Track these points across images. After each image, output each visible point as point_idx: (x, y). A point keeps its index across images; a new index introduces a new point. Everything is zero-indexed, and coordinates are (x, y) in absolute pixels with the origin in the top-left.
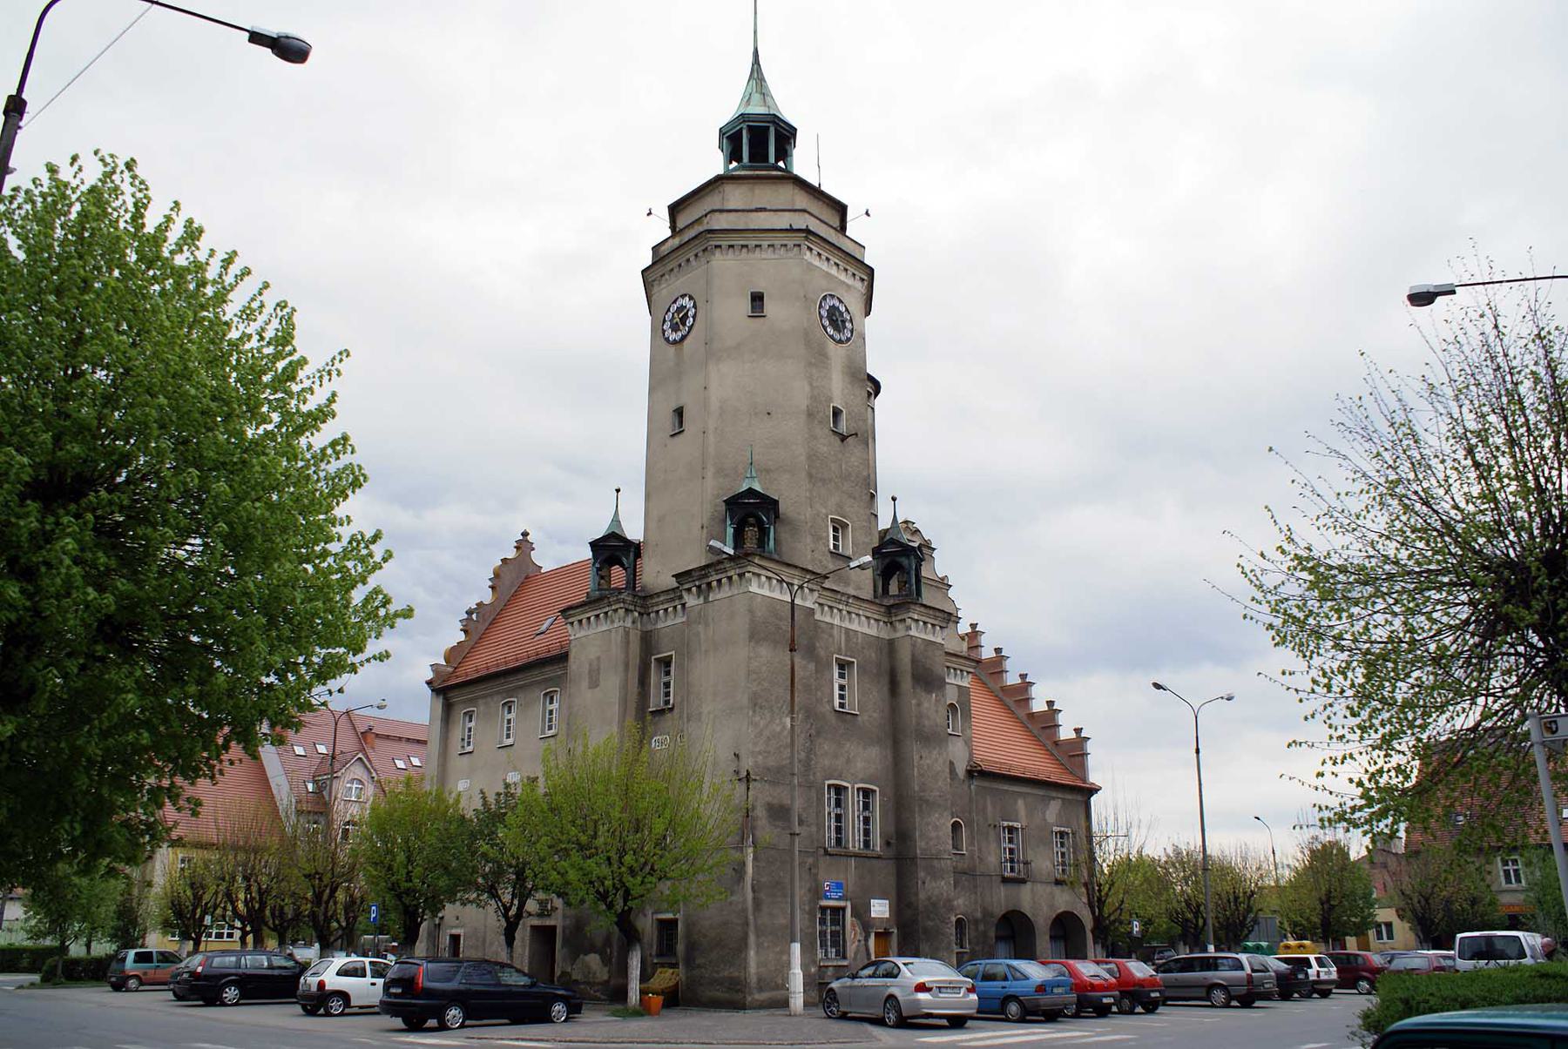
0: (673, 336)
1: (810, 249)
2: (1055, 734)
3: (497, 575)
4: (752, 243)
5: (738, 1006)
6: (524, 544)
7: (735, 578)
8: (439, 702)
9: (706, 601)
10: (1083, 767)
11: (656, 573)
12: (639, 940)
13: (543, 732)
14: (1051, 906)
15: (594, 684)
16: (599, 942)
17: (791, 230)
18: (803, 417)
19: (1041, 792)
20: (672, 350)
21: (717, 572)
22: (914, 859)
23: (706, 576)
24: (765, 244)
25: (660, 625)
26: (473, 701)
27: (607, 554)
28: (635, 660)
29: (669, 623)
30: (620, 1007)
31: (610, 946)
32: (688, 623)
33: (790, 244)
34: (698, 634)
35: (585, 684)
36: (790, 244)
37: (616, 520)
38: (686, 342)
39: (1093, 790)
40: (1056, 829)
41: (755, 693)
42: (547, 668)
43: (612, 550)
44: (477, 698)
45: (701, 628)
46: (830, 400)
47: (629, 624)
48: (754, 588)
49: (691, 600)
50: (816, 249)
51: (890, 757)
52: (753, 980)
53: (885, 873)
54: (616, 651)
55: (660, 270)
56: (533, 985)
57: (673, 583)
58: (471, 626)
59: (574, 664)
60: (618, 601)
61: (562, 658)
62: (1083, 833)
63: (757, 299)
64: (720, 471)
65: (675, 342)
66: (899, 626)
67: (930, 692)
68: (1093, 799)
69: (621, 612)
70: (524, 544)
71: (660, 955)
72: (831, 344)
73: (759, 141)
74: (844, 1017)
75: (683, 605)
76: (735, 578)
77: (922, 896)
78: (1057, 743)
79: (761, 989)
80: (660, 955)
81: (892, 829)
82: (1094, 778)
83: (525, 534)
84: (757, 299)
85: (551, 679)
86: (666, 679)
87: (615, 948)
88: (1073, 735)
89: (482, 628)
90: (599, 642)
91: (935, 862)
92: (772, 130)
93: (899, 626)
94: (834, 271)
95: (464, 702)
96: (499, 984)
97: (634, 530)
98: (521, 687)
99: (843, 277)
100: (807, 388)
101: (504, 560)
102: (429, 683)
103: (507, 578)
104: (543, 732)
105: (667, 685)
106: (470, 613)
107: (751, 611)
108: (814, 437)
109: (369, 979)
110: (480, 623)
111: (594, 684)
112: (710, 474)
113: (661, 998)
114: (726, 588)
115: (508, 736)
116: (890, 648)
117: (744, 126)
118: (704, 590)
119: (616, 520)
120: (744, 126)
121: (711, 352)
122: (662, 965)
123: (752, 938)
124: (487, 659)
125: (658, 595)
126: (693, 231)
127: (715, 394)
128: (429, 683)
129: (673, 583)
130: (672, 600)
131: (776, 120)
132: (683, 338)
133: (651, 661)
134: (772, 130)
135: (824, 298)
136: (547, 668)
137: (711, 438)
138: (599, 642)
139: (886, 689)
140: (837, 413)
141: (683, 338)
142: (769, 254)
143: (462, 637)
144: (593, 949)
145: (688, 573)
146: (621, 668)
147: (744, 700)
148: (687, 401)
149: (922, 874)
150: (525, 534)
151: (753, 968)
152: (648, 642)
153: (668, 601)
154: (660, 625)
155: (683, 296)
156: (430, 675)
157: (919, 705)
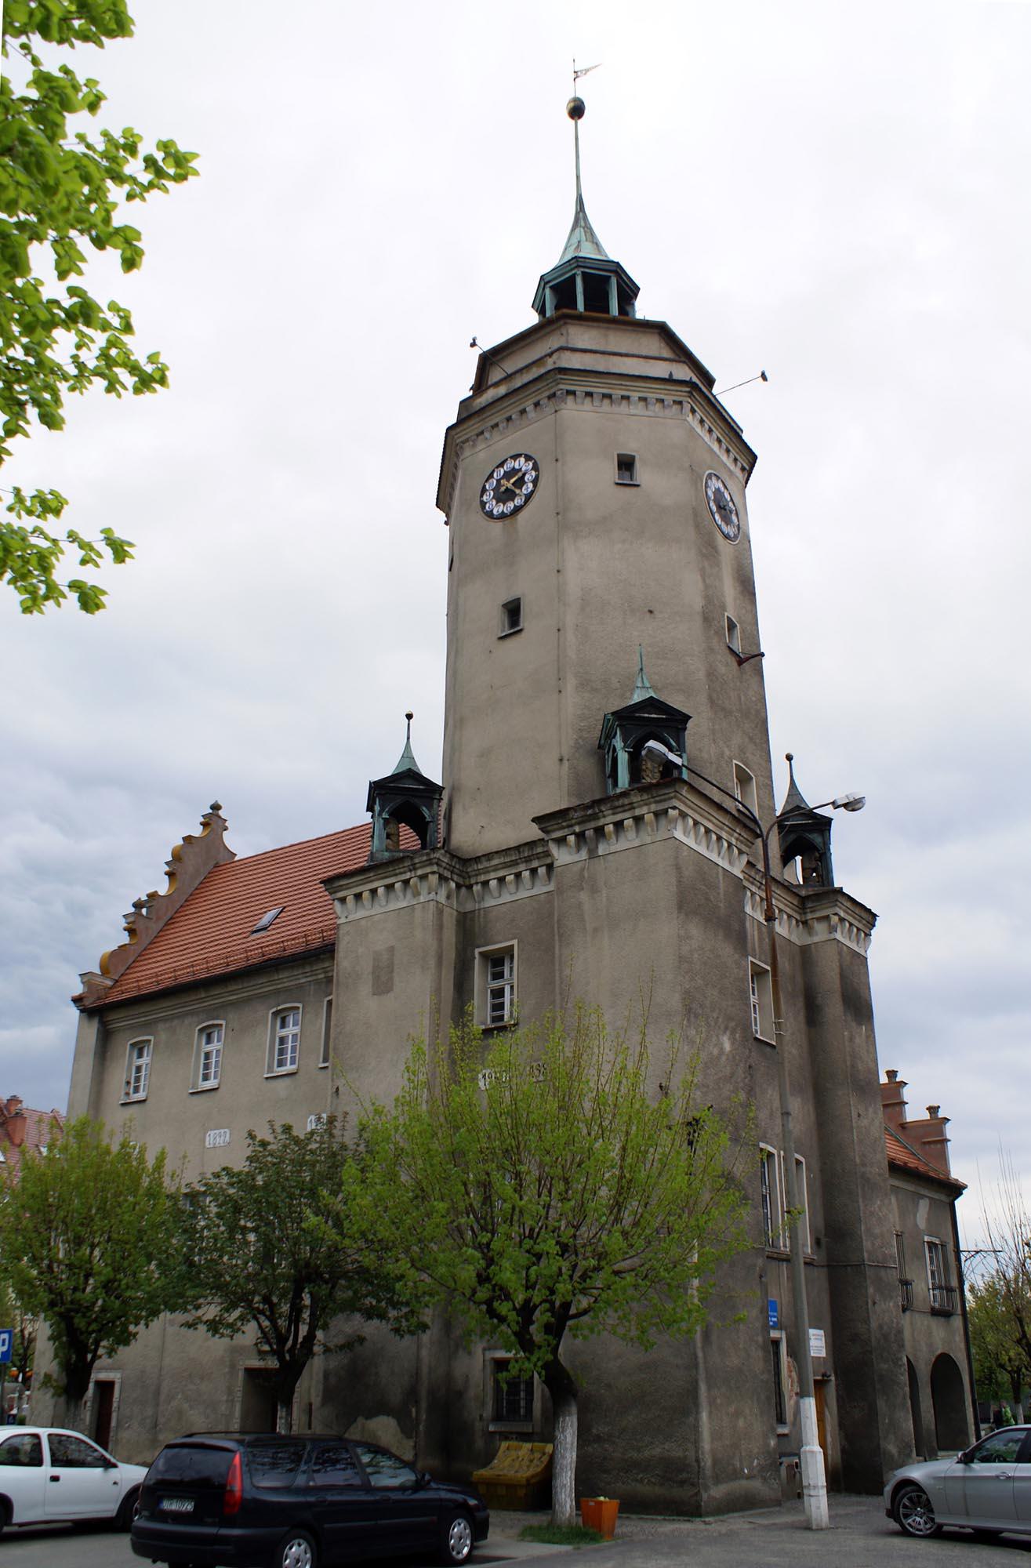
0: (498, 509)
1: (693, 411)
2: (902, 1113)
3: (177, 857)
4: (618, 393)
5: (690, 1510)
6: (213, 820)
7: (649, 817)
8: (93, 1029)
9: (593, 854)
10: (943, 1157)
11: (473, 828)
12: (575, 1396)
13: (270, 1069)
14: (930, 1346)
15: (383, 985)
16: (395, 1396)
17: (670, 380)
18: (698, 622)
19: (910, 1187)
20: (497, 526)
21: (615, 810)
22: (859, 1267)
23: (595, 817)
24: (635, 396)
25: (489, 902)
26: (147, 1027)
27: (399, 800)
28: (450, 955)
29: (506, 898)
30: (537, 1519)
31: (417, 1403)
32: (560, 890)
33: (669, 399)
34: (580, 905)
35: (365, 988)
36: (669, 399)
37: (407, 754)
38: (522, 516)
39: (957, 1189)
40: (926, 1239)
41: (687, 992)
42: (301, 967)
43: (402, 798)
44: (156, 1021)
45: (584, 896)
46: (723, 608)
47: (442, 898)
48: (678, 834)
49: (562, 856)
50: (699, 414)
51: (813, 1117)
52: (708, 1462)
53: (812, 1289)
54: (423, 935)
55: (473, 426)
56: (418, 1486)
57: (534, 832)
58: (140, 926)
59: (344, 960)
60: (430, 862)
61: (326, 951)
62: (951, 1247)
63: (626, 464)
64: (584, 684)
65: (503, 516)
66: (820, 928)
67: (860, 1024)
68: (959, 1203)
69: (434, 879)
70: (213, 820)
71: (498, 1418)
72: (720, 538)
73: (587, 291)
74: (939, 1534)
75: (550, 867)
76: (649, 817)
77: (874, 1325)
78: (904, 1126)
79: (717, 1480)
80: (498, 1418)
81: (821, 1223)
82: (957, 1171)
83: (216, 807)
84: (626, 464)
85: (287, 990)
86: (496, 984)
87: (424, 1405)
88: (927, 1116)
89: (155, 927)
90: (392, 929)
91: (883, 1273)
92: (614, 281)
93: (820, 928)
94: (715, 447)
95: (131, 1027)
96: (367, 1488)
97: (432, 770)
98: (232, 1004)
99: (724, 458)
100: (700, 585)
101: (188, 839)
102: (77, 1000)
103: (190, 863)
104: (270, 1069)
105: (498, 993)
106: (138, 905)
107: (678, 868)
108: (711, 650)
109: (47, 1470)
110: (150, 920)
111: (383, 985)
112: (571, 683)
113: (616, 1502)
114: (631, 834)
115: (206, 1078)
116: (805, 956)
117: (579, 272)
118: (590, 838)
119: (407, 754)
120: (579, 272)
121: (566, 522)
122: (505, 1436)
123: (703, 1388)
124: (169, 964)
125: (489, 856)
126: (508, 387)
127: (574, 581)
128: (77, 1000)
129: (534, 832)
130: (514, 863)
131: (617, 269)
132: (517, 510)
133: (473, 955)
134: (614, 281)
135: (710, 476)
136: (301, 967)
137: (570, 637)
138: (392, 929)
139: (802, 1017)
140: (732, 626)
141: (517, 510)
142: (638, 409)
143: (125, 939)
144: (381, 1408)
145: (562, 814)
146: (432, 962)
147: (675, 1002)
148: (527, 587)
149: (871, 1290)
150: (216, 807)
151: (706, 1445)
152: (468, 929)
153: (506, 865)
154: (489, 902)
155: (515, 457)
156: (78, 989)
157: (851, 1039)
